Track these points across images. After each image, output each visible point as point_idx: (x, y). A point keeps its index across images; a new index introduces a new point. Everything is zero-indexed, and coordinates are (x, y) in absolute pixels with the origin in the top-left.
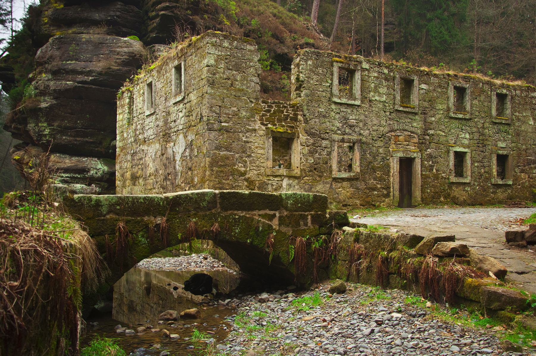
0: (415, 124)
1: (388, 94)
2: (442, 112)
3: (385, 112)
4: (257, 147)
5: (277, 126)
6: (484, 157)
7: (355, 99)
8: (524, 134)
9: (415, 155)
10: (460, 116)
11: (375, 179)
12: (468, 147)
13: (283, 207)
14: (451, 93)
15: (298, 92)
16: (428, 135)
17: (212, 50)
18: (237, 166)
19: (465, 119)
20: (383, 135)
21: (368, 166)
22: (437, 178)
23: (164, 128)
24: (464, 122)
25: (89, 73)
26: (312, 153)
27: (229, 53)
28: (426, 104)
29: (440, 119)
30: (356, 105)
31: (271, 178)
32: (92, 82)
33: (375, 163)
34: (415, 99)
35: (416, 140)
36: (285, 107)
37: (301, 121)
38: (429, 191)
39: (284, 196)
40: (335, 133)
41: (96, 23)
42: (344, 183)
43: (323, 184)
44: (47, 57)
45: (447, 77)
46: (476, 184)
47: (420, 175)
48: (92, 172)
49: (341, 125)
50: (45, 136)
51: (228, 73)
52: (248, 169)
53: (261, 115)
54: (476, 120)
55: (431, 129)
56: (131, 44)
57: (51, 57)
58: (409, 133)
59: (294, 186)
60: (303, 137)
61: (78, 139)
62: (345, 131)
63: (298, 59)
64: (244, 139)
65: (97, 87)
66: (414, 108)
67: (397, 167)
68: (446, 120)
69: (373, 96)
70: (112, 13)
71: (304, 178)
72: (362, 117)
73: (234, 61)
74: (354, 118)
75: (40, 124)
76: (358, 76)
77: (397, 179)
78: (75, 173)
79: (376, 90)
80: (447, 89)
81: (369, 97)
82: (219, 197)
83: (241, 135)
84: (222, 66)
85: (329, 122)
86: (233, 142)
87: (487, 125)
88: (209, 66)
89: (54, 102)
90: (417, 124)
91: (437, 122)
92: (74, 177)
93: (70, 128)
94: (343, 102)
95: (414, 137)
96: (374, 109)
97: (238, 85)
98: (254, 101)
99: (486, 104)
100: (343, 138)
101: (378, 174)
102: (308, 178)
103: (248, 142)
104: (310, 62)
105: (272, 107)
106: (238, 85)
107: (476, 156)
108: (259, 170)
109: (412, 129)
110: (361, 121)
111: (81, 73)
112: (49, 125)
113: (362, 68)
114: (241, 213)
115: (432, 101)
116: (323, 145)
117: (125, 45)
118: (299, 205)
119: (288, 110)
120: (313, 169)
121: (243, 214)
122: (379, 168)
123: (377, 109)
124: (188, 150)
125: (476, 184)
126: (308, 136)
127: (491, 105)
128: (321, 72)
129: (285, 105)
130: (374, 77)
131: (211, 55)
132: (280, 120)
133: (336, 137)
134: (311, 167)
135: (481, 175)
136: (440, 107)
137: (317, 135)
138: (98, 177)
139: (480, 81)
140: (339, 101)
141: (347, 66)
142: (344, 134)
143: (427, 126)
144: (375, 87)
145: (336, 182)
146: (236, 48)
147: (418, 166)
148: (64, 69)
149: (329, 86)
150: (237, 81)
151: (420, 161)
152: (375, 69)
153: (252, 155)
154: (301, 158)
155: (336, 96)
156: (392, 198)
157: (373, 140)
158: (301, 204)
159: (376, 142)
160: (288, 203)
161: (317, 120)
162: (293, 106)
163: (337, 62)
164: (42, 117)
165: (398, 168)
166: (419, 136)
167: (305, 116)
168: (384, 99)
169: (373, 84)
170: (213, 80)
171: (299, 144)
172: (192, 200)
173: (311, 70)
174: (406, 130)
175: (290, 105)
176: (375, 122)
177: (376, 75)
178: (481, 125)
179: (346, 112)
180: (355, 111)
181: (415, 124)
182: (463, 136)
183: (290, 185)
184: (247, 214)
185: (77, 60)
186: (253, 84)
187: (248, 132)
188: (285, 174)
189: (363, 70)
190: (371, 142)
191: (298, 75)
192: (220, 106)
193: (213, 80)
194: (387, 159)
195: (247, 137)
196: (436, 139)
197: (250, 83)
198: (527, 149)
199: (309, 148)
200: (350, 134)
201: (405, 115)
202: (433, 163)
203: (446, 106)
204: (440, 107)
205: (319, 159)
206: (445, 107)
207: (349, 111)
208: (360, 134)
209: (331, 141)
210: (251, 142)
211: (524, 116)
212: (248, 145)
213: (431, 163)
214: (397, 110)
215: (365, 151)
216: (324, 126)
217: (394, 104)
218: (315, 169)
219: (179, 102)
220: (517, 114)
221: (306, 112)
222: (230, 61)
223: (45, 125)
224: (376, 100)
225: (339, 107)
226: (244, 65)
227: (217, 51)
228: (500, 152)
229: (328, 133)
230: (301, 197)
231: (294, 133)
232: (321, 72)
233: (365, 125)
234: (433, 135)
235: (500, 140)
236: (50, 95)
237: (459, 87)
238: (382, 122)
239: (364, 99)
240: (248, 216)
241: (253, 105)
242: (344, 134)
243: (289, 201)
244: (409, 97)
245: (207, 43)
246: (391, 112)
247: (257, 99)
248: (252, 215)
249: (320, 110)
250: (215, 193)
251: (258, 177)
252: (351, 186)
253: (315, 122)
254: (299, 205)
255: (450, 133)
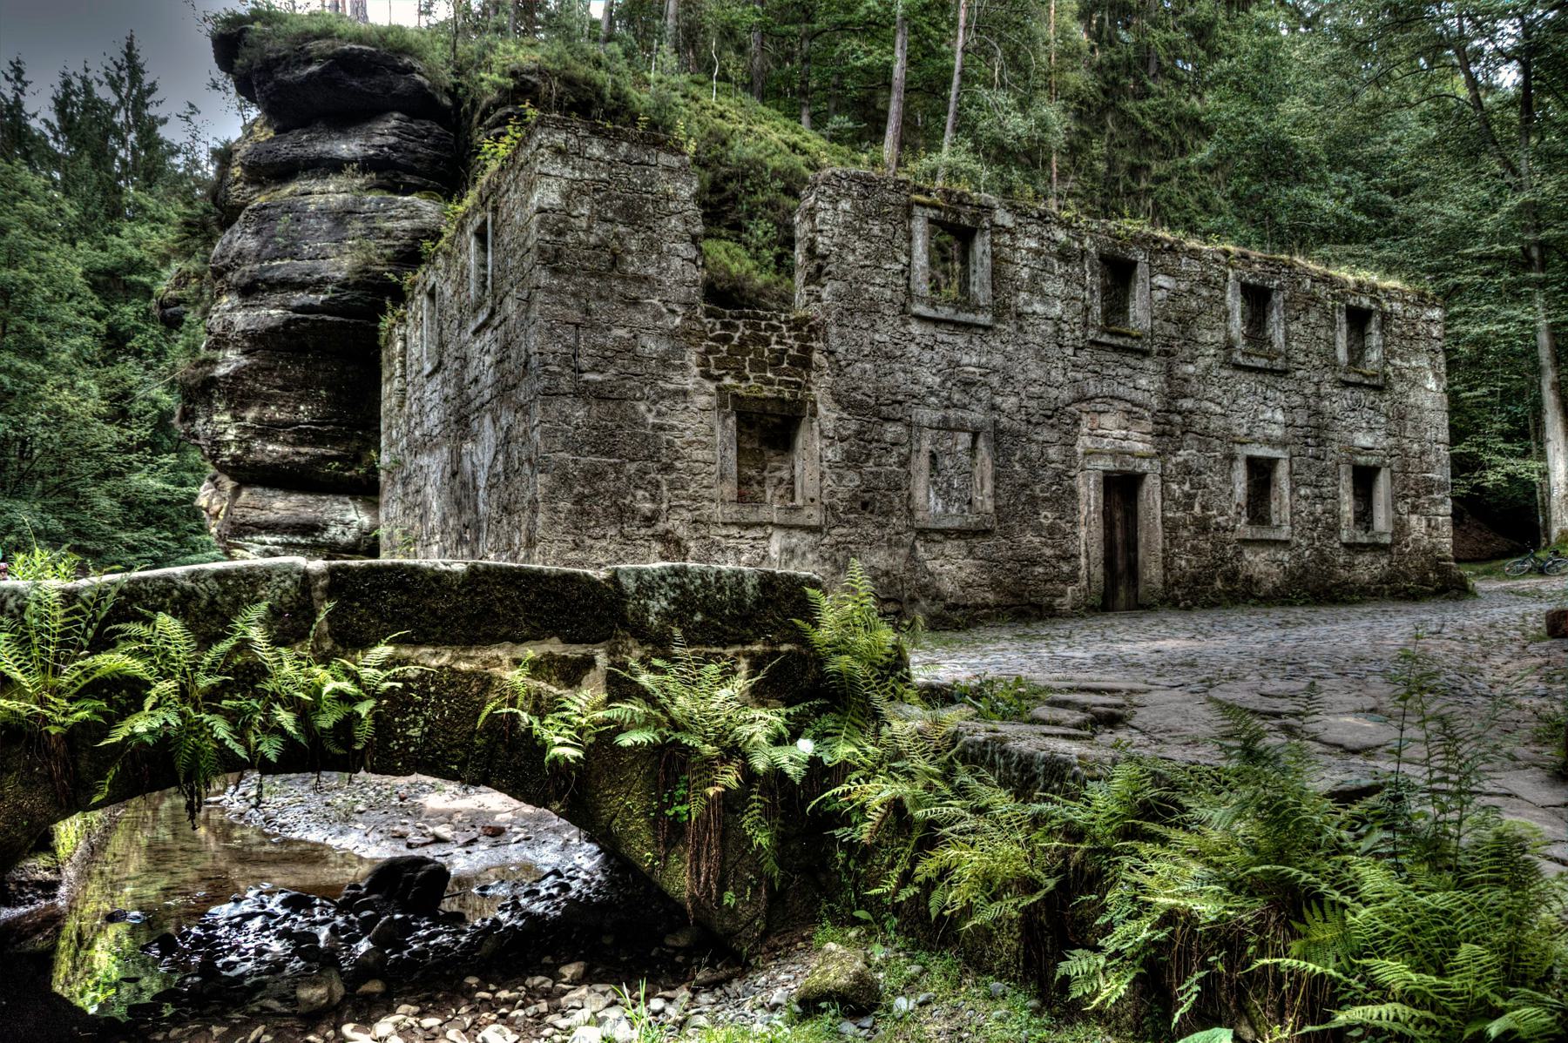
0: (1143, 382)
1: (1069, 300)
2: (1212, 351)
3: (1061, 346)
4: (690, 444)
5: (752, 382)
6: (1323, 473)
7: (976, 309)
8: (1415, 413)
9: (1146, 465)
10: (1261, 363)
11: (1038, 530)
12: (1283, 444)
13: (624, 624)
14: (1234, 302)
15: (812, 287)
16: (1180, 413)
17: (556, 168)
18: (630, 498)
19: (1272, 371)
20: (1056, 410)
21: (1017, 495)
22: (1205, 530)
23: (457, 402)
24: (1268, 379)
25: (318, 286)
26: (852, 461)
27: (604, 175)
28: (1170, 329)
29: (1208, 368)
30: (979, 326)
31: (734, 531)
32: (325, 308)
33: (1037, 489)
34: (1139, 313)
35: (1148, 425)
36: (775, 329)
37: (820, 368)
38: (1183, 563)
39: (630, 584)
40: (922, 401)
41: (336, 166)
42: (948, 544)
43: (890, 546)
44: (231, 254)
45: (1222, 258)
46: (1304, 543)
47: (1159, 521)
48: (333, 531)
49: (938, 380)
50: (227, 444)
51: (600, 230)
52: (664, 506)
53: (702, 349)
54: (1299, 374)
55: (1185, 397)
56: (418, 209)
57: (240, 254)
58: (1129, 405)
59: (804, 554)
60: (828, 414)
61: (303, 450)
62: (949, 399)
63: (812, 199)
64: (651, 419)
65: (338, 319)
66: (1138, 338)
67: (1096, 499)
68: (1225, 373)
69: (1027, 303)
70: (377, 140)
71: (833, 532)
72: (998, 360)
73: (618, 197)
74: (974, 360)
75: (215, 418)
76: (981, 246)
77: (1098, 531)
78: (294, 534)
79: (1034, 286)
80: (1223, 290)
81: (1016, 305)
82: (322, 589)
83: (642, 407)
84: (585, 210)
85: (905, 371)
86: (619, 426)
87: (1326, 389)
88: (545, 211)
89: (244, 361)
90: (1147, 383)
91: (1202, 379)
92: (290, 544)
93: (286, 424)
94: (942, 316)
95: (1142, 418)
96: (1030, 337)
97: (633, 265)
98: (680, 310)
99: (1322, 333)
100: (945, 419)
101: (1047, 516)
102: (844, 531)
103: (661, 428)
104: (845, 205)
105: (737, 328)
106: (633, 265)
107: (1303, 469)
108: (697, 509)
109: (1139, 396)
110: (995, 371)
111: (302, 286)
112: (235, 418)
113: (993, 224)
114: (435, 655)
115: (1185, 322)
116: (889, 437)
117: (406, 213)
118: (698, 617)
119: (782, 337)
120: (857, 505)
121: (444, 660)
122: (1045, 499)
123: (1038, 340)
124: (500, 457)
125: (1304, 543)
126: (844, 409)
127: (1334, 337)
128: (876, 230)
129: (775, 322)
130: (1029, 250)
131: (551, 180)
132: (758, 366)
133: (926, 415)
134: (854, 498)
135: (1317, 520)
136: (1208, 337)
137: (869, 407)
138: (348, 543)
139: (1306, 272)
140: (931, 313)
141: (950, 218)
142: (947, 407)
143: (1175, 388)
144: (1033, 278)
145: (927, 541)
146: (627, 160)
147: (1151, 498)
148: (265, 281)
149: (903, 272)
150: (630, 252)
151: (1158, 481)
152: (1029, 228)
153: (678, 464)
154: (822, 475)
155: (921, 299)
156: (1084, 583)
157: (1029, 422)
158: (707, 612)
159: (1038, 429)
160: (646, 609)
161: (868, 366)
162: (797, 325)
163: (923, 205)
164: (220, 400)
165: (1101, 501)
166: (1154, 415)
167: (832, 353)
168: (1057, 309)
169: (1026, 270)
170: (557, 251)
171: (817, 433)
172: (191, 605)
173: (847, 225)
174: (1120, 399)
175: (787, 322)
176: (1036, 373)
177: (1034, 244)
178: (1314, 389)
179: (953, 346)
180: (976, 341)
181: (1143, 382)
182: (1268, 415)
183: (791, 552)
184: (458, 659)
185: (293, 256)
186: (677, 263)
187: (663, 398)
188: (775, 520)
189: (999, 229)
190: (1024, 428)
191: (812, 241)
192: (577, 326)
193: (557, 251)
194: (1071, 478)
195: (659, 414)
196: (1200, 422)
197: (668, 261)
198: (1423, 453)
199: (846, 445)
200: (964, 407)
201: (1115, 356)
202: (1192, 487)
203: (1223, 334)
204: (1208, 337)
205: (877, 475)
206: (1220, 337)
207: (961, 341)
208: (994, 408)
209: (909, 425)
210: (672, 427)
211: (1414, 369)
212: (665, 436)
213: (1187, 487)
214: (1093, 342)
215: (1008, 455)
216: (887, 381)
217: (1086, 324)
218: (865, 505)
219: (484, 325)
220: (1398, 362)
221: (835, 342)
222: (609, 197)
223: (227, 418)
224: (1034, 313)
225: (931, 329)
226: (650, 208)
227: (568, 169)
228: (1361, 460)
229: (900, 403)
230: (706, 585)
231: (803, 402)
232: (876, 230)
233: (1007, 380)
234: (1191, 412)
235: (1359, 429)
236: (235, 344)
237: (1255, 285)
238: (1053, 373)
239: (1001, 310)
240: (463, 666)
241: (678, 321)
242: (950, 404)
243: (651, 603)
244: (1124, 310)
245: (540, 146)
246: (1076, 348)
247: (690, 305)
248: (485, 663)
249: (877, 337)
250: (305, 574)
251: (696, 530)
252: (970, 552)
253: (865, 371)
254: (698, 617)
255: (1235, 407)
